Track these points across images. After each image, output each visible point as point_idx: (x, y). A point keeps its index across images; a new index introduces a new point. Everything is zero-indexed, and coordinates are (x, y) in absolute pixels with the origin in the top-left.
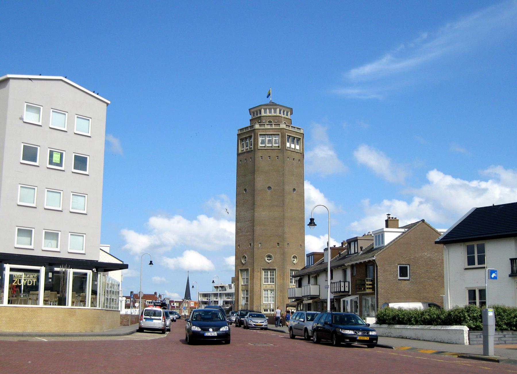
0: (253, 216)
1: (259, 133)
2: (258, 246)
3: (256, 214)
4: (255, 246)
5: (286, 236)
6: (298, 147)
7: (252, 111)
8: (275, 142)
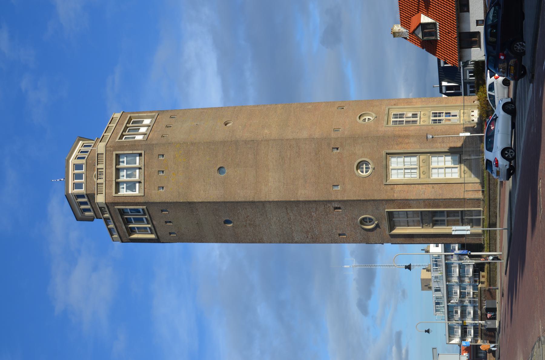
0: (277, 203)
1: (114, 195)
2: (338, 194)
3: (273, 197)
4: (340, 198)
5: (317, 135)
7: (79, 214)
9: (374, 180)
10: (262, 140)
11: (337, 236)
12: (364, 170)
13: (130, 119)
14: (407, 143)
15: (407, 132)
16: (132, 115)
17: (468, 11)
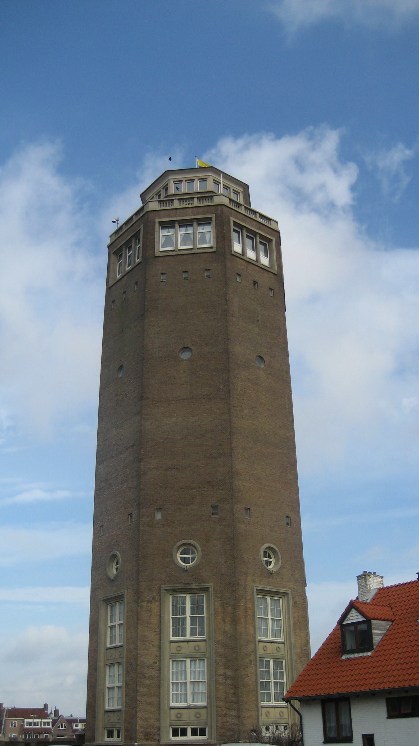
1: (157, 221)
6: (265, 261)
8: (204, 237)
9: (168, 570)
10: (229, 404)
11: (101, 524)
12: (185, 556)
13: (270, 241)
14: (224, 620)
15: (243, 620)
16: (274, 242)
17: (390, 716)
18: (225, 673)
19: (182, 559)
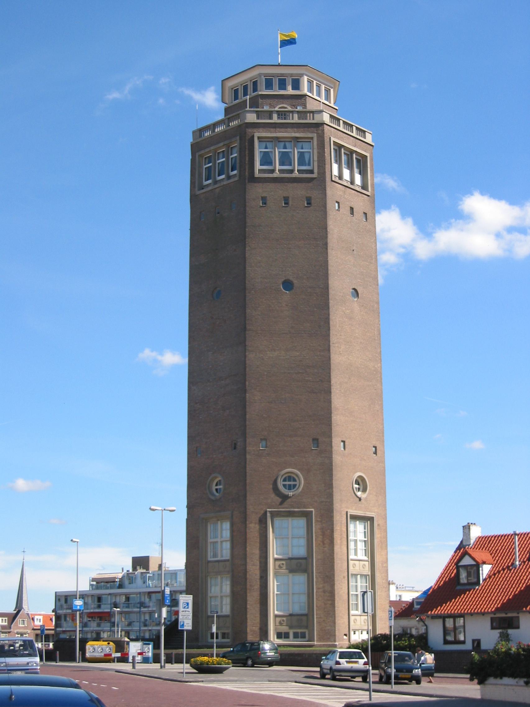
0: (243, 364)
12: (287, 483)
18: (323, 587)
19: (284, 486)
